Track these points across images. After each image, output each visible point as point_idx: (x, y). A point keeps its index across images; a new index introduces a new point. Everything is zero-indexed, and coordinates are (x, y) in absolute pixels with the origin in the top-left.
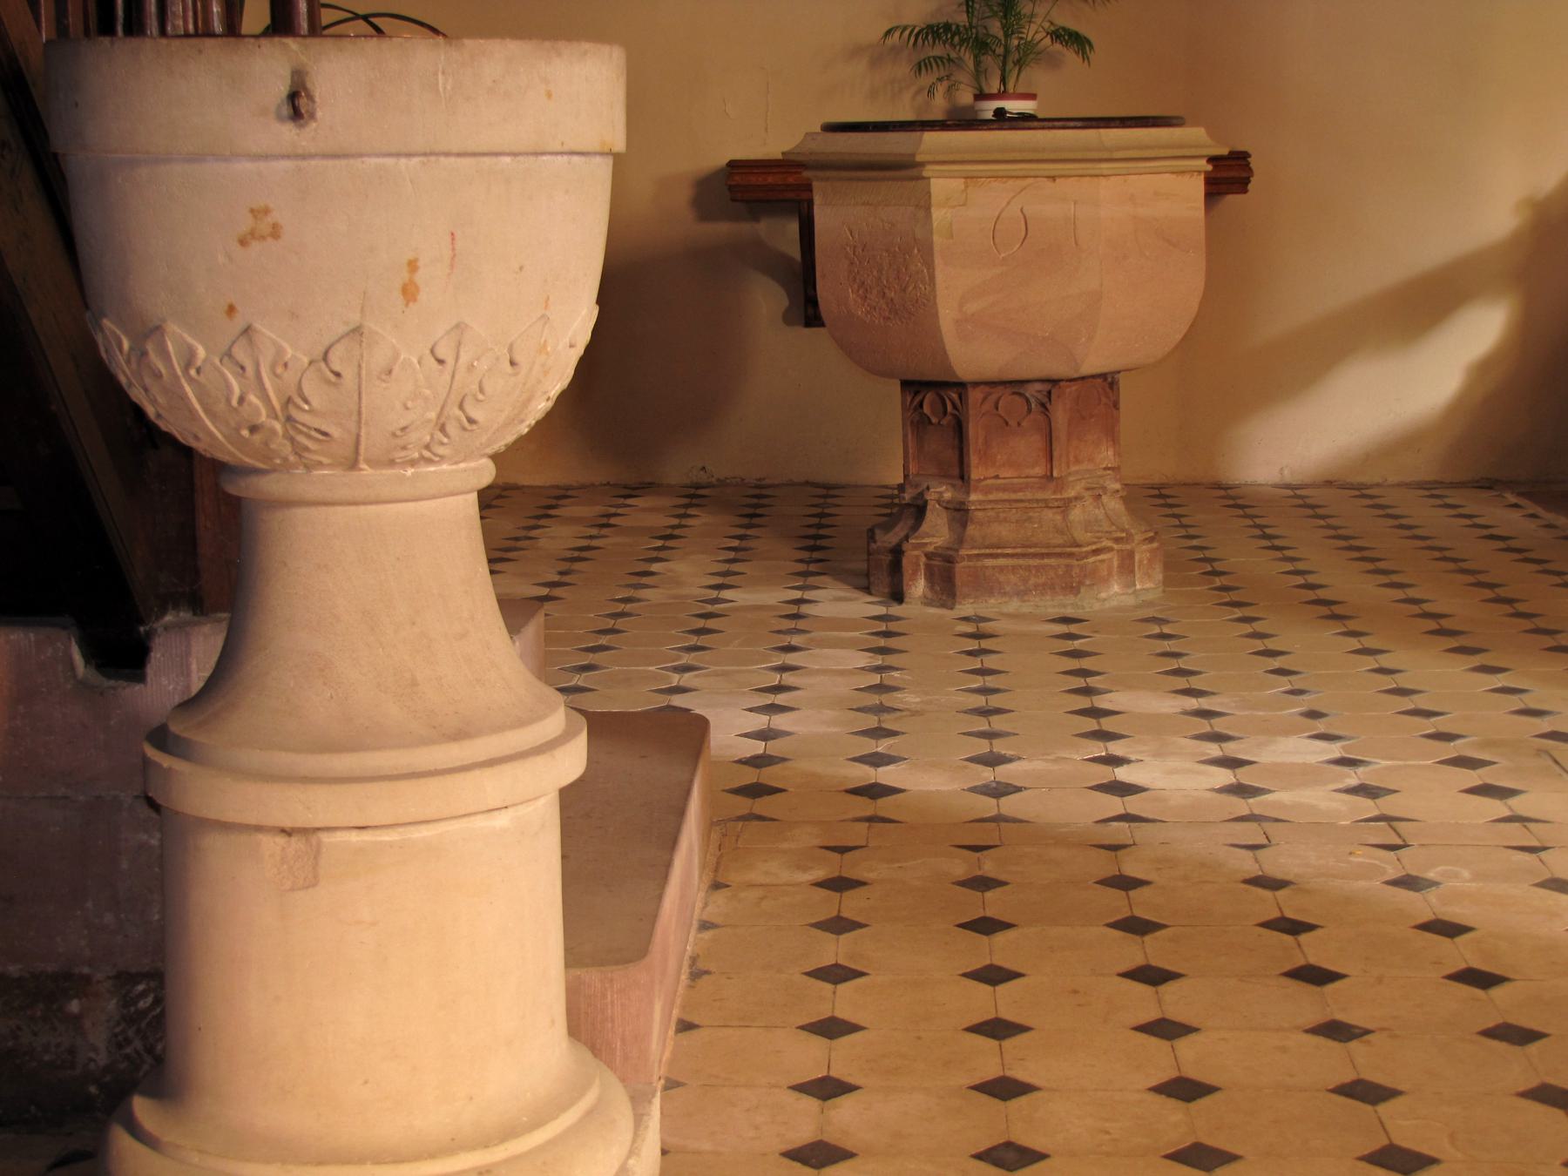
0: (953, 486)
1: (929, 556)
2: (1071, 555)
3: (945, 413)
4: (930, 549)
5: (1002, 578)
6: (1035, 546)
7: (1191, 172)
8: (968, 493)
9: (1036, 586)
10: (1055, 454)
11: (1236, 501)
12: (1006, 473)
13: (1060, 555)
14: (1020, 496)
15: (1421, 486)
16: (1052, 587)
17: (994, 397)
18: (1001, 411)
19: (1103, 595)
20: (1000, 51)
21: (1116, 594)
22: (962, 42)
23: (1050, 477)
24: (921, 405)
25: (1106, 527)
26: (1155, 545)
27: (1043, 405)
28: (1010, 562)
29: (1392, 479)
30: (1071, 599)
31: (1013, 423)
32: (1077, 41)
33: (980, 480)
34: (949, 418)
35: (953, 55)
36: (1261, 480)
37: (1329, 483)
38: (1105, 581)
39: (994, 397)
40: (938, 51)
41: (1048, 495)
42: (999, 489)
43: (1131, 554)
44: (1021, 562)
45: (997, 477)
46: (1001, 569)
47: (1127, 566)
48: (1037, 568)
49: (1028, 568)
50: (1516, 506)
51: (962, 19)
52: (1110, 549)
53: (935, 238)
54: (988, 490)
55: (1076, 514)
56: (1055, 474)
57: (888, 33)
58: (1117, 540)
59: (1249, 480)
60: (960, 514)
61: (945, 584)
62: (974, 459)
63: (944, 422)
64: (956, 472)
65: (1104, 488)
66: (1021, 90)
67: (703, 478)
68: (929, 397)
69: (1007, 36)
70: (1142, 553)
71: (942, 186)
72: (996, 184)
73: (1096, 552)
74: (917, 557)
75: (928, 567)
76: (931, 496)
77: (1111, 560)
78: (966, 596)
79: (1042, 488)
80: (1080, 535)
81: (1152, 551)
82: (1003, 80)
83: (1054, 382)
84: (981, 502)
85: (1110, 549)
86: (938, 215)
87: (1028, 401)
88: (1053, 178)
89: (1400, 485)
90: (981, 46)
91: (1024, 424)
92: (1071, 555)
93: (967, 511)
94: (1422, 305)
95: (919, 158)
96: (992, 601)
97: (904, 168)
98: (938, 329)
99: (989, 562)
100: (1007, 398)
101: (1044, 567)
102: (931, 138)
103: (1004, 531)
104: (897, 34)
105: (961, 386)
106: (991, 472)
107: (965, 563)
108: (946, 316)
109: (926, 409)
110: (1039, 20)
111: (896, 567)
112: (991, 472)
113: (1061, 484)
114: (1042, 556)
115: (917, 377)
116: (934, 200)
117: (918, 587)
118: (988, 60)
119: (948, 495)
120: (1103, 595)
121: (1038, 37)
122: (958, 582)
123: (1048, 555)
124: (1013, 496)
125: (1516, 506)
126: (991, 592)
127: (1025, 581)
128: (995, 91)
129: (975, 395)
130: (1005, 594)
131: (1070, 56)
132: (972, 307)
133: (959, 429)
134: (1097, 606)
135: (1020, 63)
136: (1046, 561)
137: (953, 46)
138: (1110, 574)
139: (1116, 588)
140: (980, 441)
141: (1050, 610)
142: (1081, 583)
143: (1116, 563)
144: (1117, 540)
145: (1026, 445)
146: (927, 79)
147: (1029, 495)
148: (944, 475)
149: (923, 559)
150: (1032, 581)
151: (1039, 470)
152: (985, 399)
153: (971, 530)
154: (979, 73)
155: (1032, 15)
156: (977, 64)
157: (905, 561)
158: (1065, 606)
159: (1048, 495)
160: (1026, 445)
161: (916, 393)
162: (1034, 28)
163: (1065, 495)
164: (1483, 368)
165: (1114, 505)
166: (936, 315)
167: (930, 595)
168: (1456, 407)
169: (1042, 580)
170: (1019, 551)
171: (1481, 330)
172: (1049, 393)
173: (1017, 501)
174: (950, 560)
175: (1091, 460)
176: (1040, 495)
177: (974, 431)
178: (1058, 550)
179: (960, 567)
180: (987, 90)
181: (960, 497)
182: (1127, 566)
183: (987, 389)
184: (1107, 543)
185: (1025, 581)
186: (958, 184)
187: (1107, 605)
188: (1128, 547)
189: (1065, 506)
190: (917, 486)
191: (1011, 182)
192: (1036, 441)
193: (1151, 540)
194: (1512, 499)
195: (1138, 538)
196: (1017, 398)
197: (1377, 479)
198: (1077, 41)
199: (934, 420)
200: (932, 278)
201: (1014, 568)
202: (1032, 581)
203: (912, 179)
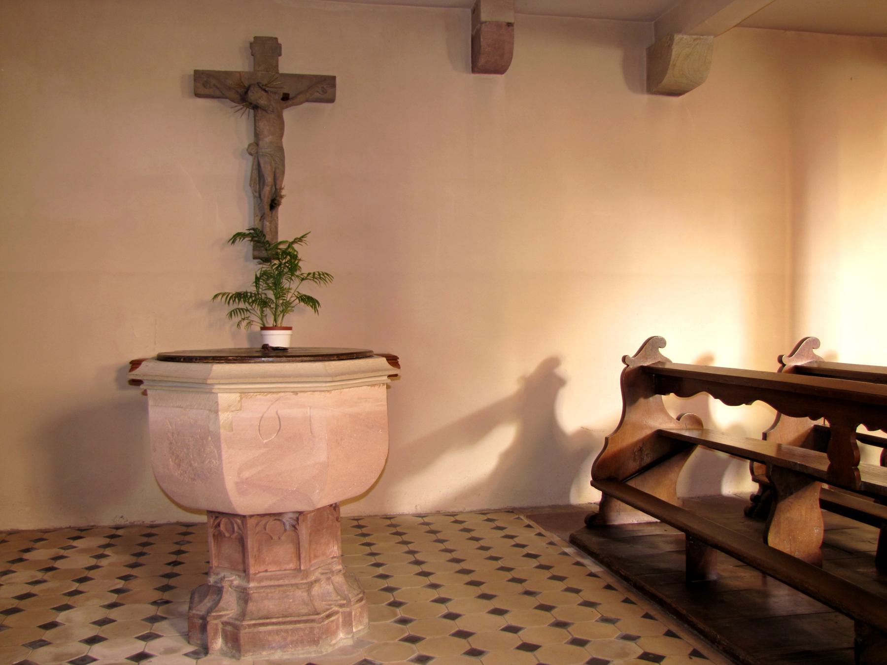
0: (240, 576)
1: (225, 624)
2: (313, 621)
3: (233, 531)
4: (225, 619)
5: (270, 638)
6: (291, 615)
7: (379, 385)
8: (248, 582)
9: (292, 642)
10: (303, 556)
11: (394, 526)
12: (272, 568)
13: (306, 621)
14: (281, 582)
15: (483, 513)
16: (302, 642)
17: (264, 522)
18: (267, 531)
19: (334, 642)
20: (273, 306)
21: (342, 639)
22: (253, 302)
23: (299, 570)
24: (219, 525)
25: (334, 596)
26: (363, 602)
27: (294, 526)
28: (275, 627)
29: (468, 509)
30: (314, 648)
31: (275, 538)
32: (310, 301)
33: (256, 574)
34: (236, 534)
35: (249, 307)
36: (406, 512)
37: (438, 513)
38: (334, 633)
39: (264, 522)
40: (242, 305)
41: (298, 581)
42: (267, 578)
43: (350, 614)
44: (282, 627)
45: (266, 571)
46: (270, 633)
47: (348, 622)
48: (293, 630)
49: (287, 631)
50: (529, 526)
51: (253, 289)
52: (337, 613)
53: (222, 431)
54: (261, 580)
55: (316, 590)
56: (302, 568)
57: (216, 296)
58: (341, 606)
59: (401, 512)
60: (244, 596)
61: (234, 642)
62: (251, 561)
63: (233, 536)
64: (241, 567)
65: (332, 572)
66: (284, 325)
67: (122, 522)
68: (224, 521)
69: (277, 298)
70: (356, 609)
71: (225, 398)
72: (260, 397)
73: (328, 616)
74: (216, 625)
75: (224, 631)
76: (226, 584)
77: (338, 619)
78: (249, 651)
79: (295, 577)
80: (320, 605)
81: (361, 607)
82: (275, 320)
83: (300, 513)
84: (257, 588)
85: (337, 613)
86: (223, 417)
87: (284, 524)
88: (296, 393)
89: (471, 512)
90: (264, 303)
91: (283, 538)
92: (313, 621)
93: (248, 594)
94: (478, 426)
95: (209, 382)
96: (264, 653)
97: (202, 386)
98: (225, 488)
99: (262, 629)
100: (271, 523)
101: (297, 629)
102: (219, 369)
103: (271, 605)
104: (220, 297)
105: (243, 517)
106: (263, 568)
107: (247, 630)
108: (230, 480)
109: (222, 528)
110: (292, 291)
111: (204, 628)
112: (263, 568)
113: (307, 574)
114: (296, 622)
115: (215, 510)
116: (220, 407)
117: (218, 643)
118: (267, 311)
119: (236, 583)
120: (334, 642)
121: (292, 299)
122: (242, 642)
123: (299, 622)
124: (276, 583)
125: (529, 526)
126: (263, 647)
127: (285, 639)
128: (271, 325)
129: (251, 522)
130: (272, 648)
131: (309, 309)
132: (246, 474)
133: (242, 542)
134: (330, 650)
135: (284, 312)
136: (298, 625)
137: (249, 303)
138: (338, 628)
139: (341, 635)
140: (255, 549)
141: (301, 656)
142: (320, 638)
143: (341, 620)
144: (341, 606)
145: (283, 551)
146: (236, 319)
147: (286, 582)
148: (233, 568)
149: (220, 626)
150: (289, 639)
151: (292, 566)
152: (257, 524)
153: (251, 606)
154: (263, 317)
155: (289, 289)
156: (262, 312)
157: (209, 628)
158: (310, 653)
159: (298, 581)
160: (283, 551)
161: (217, 517)
162: (289, 295)
163: (309, 580)
164: (506, 455)
165: (339, 579)
166: (223, 479)
167: (225, 648)
168: (496, 473)
169: (295, 638)
170: (280, 620)
171: (505, 437)
172: (298, 518)
173: (279, 586)
174: (236, 628)
175: (324, 554)
176: (293, 581)
177: (250, 543)
178: (305, 618)
179: (244, 634)
180: (267, 325)
181: (244, 584)
182: (348, 622)
183: (259, 518)
184: (336, 608)
185: (285, 639)
186: (235, 397)
187: (336, 647)
188: (348, 609)
189: (311, 585)
190: (218, 574)
191: (269, 395)
192: (290, 548)
193: (361, 600)
194: (527, 522)
195: (353, 600)
196: (278, 522)
197: (461, 509)
198: (310, 301)
199: (227, 535)
200: (220, 456)
201: (277, 632)
202: (289, 639)
203: (207, 393)
